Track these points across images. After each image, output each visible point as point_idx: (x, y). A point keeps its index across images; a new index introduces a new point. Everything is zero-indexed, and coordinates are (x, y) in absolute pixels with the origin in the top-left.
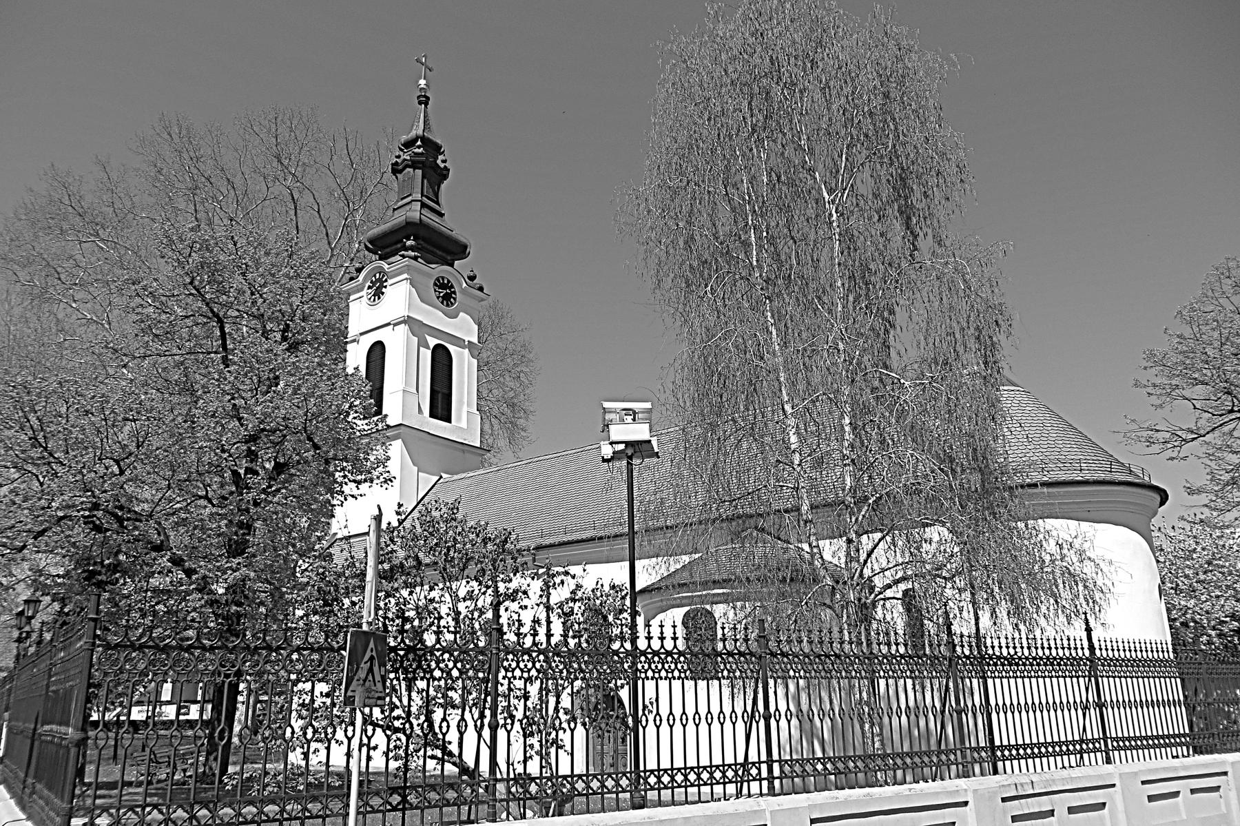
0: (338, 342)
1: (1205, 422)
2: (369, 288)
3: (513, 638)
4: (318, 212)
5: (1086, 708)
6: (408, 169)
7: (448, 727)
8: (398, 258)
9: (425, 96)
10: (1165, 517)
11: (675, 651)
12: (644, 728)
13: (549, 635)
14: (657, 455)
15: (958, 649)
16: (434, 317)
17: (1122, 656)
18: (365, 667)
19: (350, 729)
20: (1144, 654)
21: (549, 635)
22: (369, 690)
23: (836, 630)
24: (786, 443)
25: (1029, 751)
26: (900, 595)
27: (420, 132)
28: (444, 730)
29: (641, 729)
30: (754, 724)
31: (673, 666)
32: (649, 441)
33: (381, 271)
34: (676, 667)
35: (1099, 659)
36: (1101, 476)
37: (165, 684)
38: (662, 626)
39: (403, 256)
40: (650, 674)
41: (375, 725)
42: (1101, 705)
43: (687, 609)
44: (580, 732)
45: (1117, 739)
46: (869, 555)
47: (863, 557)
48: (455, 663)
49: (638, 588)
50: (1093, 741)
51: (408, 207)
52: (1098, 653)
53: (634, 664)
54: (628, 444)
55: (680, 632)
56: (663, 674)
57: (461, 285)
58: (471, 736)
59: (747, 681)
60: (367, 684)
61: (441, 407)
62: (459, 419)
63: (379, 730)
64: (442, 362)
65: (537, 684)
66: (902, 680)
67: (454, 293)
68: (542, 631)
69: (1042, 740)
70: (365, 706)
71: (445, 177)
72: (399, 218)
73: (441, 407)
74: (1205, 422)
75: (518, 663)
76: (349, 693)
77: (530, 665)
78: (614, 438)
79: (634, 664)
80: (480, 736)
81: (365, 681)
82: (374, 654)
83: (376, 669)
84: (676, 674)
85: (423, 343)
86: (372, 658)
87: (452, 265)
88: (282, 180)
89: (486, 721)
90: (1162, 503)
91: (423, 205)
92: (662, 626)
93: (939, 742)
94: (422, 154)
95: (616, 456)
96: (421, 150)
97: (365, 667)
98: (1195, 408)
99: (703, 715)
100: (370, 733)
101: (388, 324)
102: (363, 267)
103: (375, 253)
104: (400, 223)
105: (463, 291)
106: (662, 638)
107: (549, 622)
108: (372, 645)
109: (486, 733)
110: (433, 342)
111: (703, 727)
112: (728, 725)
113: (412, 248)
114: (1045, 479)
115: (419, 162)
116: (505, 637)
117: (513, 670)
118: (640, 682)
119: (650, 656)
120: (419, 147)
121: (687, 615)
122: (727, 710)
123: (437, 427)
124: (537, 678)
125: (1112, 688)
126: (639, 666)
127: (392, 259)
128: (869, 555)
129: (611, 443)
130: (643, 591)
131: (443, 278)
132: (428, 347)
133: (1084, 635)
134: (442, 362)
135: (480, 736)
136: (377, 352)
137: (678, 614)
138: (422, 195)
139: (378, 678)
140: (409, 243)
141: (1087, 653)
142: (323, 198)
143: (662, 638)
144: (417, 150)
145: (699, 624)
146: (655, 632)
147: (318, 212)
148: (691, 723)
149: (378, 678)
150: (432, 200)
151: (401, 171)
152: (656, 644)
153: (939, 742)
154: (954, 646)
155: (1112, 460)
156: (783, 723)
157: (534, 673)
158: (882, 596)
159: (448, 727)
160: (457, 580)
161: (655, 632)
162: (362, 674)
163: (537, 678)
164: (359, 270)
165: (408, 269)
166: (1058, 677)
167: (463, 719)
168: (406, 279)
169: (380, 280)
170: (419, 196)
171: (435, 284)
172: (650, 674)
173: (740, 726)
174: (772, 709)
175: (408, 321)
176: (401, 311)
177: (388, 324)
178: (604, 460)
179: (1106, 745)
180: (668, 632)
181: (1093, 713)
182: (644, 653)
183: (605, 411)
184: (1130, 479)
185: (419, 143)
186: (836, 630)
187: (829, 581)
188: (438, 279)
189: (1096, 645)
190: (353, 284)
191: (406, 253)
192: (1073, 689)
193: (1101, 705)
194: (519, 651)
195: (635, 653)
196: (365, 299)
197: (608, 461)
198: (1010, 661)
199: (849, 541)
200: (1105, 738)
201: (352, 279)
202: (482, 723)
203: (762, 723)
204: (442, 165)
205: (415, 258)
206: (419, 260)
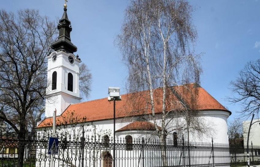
0: (45, 71)
1: (241, 97)
2: (53, 58)
3: (88, 140)
4: (40, 38)
5: (210, 157)
6: (62, 28)
7: (73, 159)
8: (59, 50)
9: (66, 9)
10: (231, 118)
11: (74, 142)
12: (116, 160)
13: (95, 140)
14: (121, 100)
15: (185, 145)
16: (68, 65)
17: (201, 146)
18: (53, 146)
19: (50, 159)
20: (219, 146)
21: (95, 140)
22: (54, 151)
23: (159, 140)
24: (150, 99)
25: (206, 165)
26: (173, 133)
27: (65, 18)
28: (72, 160)
29: (116, 160)
30: (140, 160)
31: (120, 147)
32: (119, 97)
33: (55, 53)
34: (74, 146)
35: (167, 146)
36: (218, 108)
37: (66, 149)
38: (121, 138)
39: (61, 50)
40: (118, 149)
41: (56, 158)
42: (213, 157)
43: (127, 135)
44: (102, 161)
45: (216, 164)
46: (167, 124)
47: (166, 124)
48: (74, 145)
49: (116, 130)
50: (211, 164)
51: (62, 38)
52: (214, 146)
53: (114, 146)
54: (115, 97)
55: (173, 142)
56: (121, 149)
57: (75, 58)
58: (78, 161)
59: (47, 149)
60: (54, 149)
61: (70, 88)
62: (75, 91)
63: (57, 160)
64: (70, 77)
65: (93, 150)
66: (138, 151)
67: (73, 60)
68: (94, 139)
69: (202, 164)
70: (53, 154)
71: (71, 30)
72: (60, 40)
73: (70, 88)
74: (241, 97)
75: (92, 146)
76: (49, 151)
77: (91, 146)
78: (111, 95)
79: (114, 146)
80: (80, 161)
81: (53, 149)
82: (55, 143)
83: (56, 146)
84: (137, 149)
85: (66, 72)
86: (55, 144)
87: (73, 53)
88: (30, 28)
89: (81, 158)
90: (230, 115)
91: (66, 38)
92: (121, 138)
93: (179, 164)
94: (65, 24)
95: (112, 100)
96: (65, 23)
97: (53, 146)
98: (239, 94)
99: (124, 158)
100: (54, 160)
101: (57, 67)
102: (51, 53)
103: (54, 49)
104: (60, 42)
105: (75, 60)
106: (118, 141)
107: (95, 137)
108: (55, 141)
109: (81, 160)
110: (68, 72)
111: (127, 160)
112: (129, 160)
113: (63, 48)
114: (206, 109)
115: (64, 26)
116: (85, 140)
117: (87, 147)
118: (116, 150)
119: (92, 144)
120: (64, 22)
121: (126, 136)
122: (135, 156)
123: (69, 92)
124: (75, 149)
125: (216, 153)
126: (116, 147)
127: (58, 51)
128: (167, 124)
129: (110, 97)
130: (118, 131)
131: (71, 56)
132: (67, 73)
133: (251, 145)
134: (70, 77)
135: (80, 161)
136: (55, 74)
137: (124, 136)
138: (65, 35)
139: (56, 148)
140: (62, 47)
141: (212, 146)
142: (41, 34)
143: (121, 141)
144: (64, 23)
145: (129, 139)
146: (119, 140)
147: (40, 38)
148: (124, 159)
149: (56, 148)
150: (68, 36)
151: (60, 28)
152: (119, 142)
153: (179, 164)
154: (184, 144)
155: (221, 105)
156: (88, 161)
157: (92, 148)
158: (169, 133)
159: (73, 159)
160: (75, 127)
161: (119, 140)
162: (52, 147)
163: (75, 149)
164: (50, 53)
165: (62, 53)
166: (201, 151)
167: (76, 157)
168: (62, 56)
169: (55, 56)
170: (64, 35)
171: (69, 58)
172: (118, 149)
173: (137, 160)
174: (144, 157)
175: (63, 67)
176: (61, 64)
177: (57, 67)
178: (109, 101)
179: (214, 165)
180: (122, 140)
181: (212, 158)
182: (117, 144)
183: (109, 89)
184: (224, 109)
185: (64, 21)
186: (159, 140)
187: (157, 130)
188: (69, 57)
189: (214, 145)
190: (49, 57)
191: (61, 49)
192: (208, 153)
193: (213, 157)
194: (88, 143)
195: (114, 144)
196: (52, 61)
197: (109, 101)
198: (196, 147)
199: (163, 121)
200: (214, 164)
201: (48, 55)
202: (80, 158)
203: (142, 159)
204: (70, 27)
205: (64, 51)
206: (65, 51)
